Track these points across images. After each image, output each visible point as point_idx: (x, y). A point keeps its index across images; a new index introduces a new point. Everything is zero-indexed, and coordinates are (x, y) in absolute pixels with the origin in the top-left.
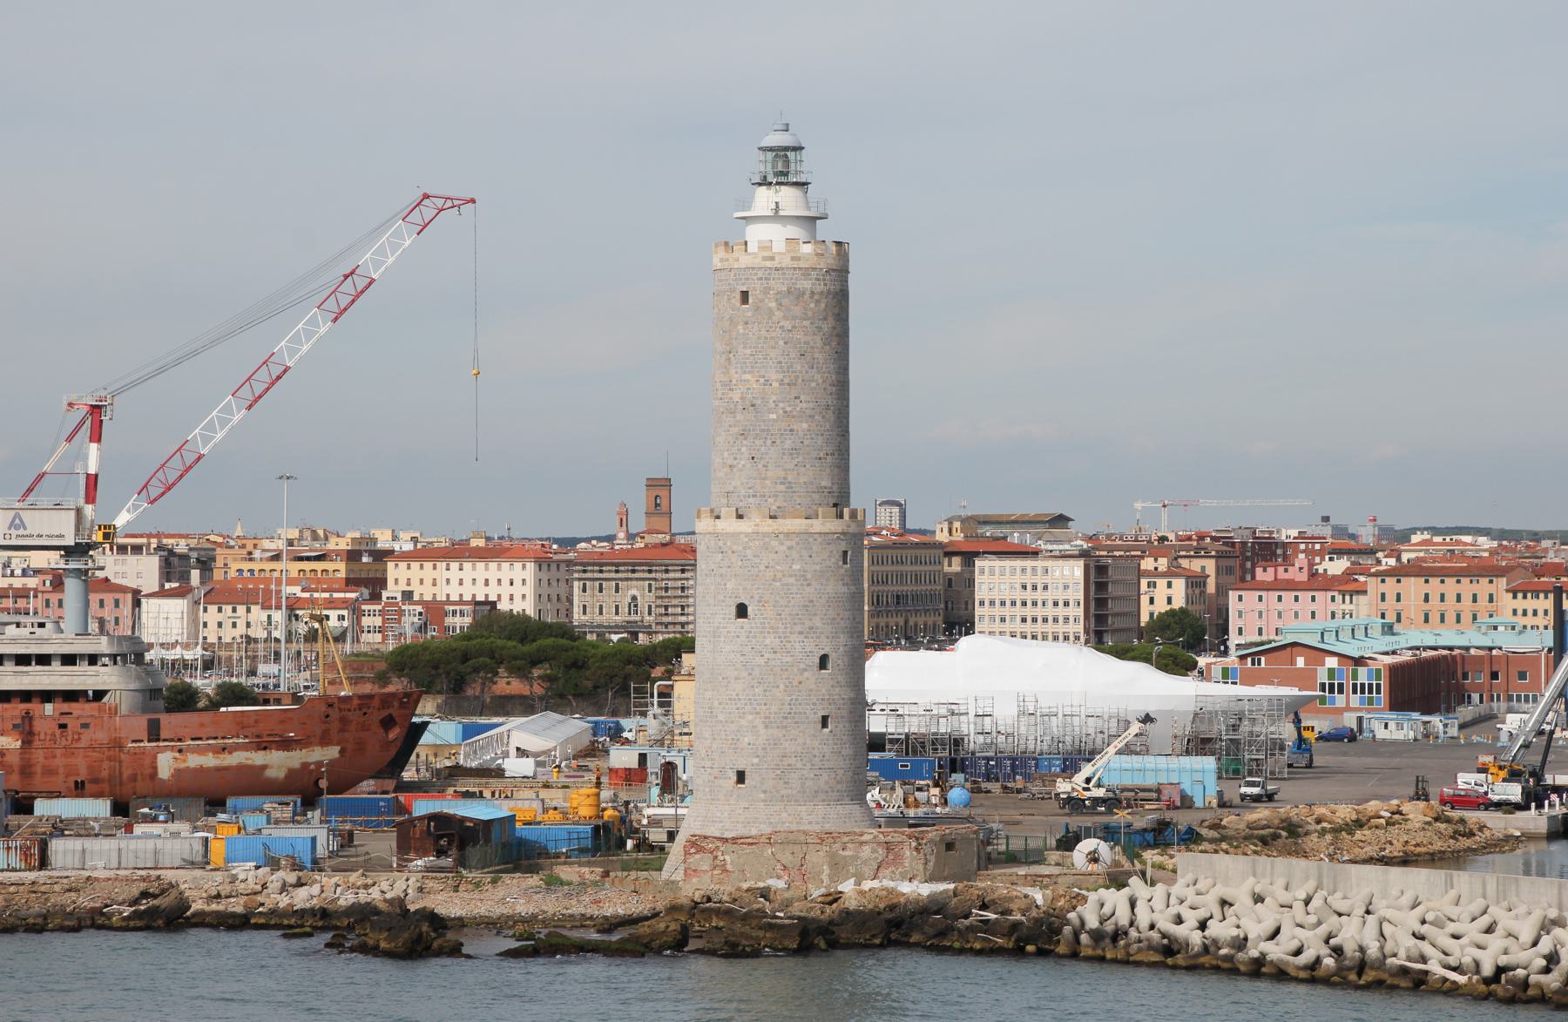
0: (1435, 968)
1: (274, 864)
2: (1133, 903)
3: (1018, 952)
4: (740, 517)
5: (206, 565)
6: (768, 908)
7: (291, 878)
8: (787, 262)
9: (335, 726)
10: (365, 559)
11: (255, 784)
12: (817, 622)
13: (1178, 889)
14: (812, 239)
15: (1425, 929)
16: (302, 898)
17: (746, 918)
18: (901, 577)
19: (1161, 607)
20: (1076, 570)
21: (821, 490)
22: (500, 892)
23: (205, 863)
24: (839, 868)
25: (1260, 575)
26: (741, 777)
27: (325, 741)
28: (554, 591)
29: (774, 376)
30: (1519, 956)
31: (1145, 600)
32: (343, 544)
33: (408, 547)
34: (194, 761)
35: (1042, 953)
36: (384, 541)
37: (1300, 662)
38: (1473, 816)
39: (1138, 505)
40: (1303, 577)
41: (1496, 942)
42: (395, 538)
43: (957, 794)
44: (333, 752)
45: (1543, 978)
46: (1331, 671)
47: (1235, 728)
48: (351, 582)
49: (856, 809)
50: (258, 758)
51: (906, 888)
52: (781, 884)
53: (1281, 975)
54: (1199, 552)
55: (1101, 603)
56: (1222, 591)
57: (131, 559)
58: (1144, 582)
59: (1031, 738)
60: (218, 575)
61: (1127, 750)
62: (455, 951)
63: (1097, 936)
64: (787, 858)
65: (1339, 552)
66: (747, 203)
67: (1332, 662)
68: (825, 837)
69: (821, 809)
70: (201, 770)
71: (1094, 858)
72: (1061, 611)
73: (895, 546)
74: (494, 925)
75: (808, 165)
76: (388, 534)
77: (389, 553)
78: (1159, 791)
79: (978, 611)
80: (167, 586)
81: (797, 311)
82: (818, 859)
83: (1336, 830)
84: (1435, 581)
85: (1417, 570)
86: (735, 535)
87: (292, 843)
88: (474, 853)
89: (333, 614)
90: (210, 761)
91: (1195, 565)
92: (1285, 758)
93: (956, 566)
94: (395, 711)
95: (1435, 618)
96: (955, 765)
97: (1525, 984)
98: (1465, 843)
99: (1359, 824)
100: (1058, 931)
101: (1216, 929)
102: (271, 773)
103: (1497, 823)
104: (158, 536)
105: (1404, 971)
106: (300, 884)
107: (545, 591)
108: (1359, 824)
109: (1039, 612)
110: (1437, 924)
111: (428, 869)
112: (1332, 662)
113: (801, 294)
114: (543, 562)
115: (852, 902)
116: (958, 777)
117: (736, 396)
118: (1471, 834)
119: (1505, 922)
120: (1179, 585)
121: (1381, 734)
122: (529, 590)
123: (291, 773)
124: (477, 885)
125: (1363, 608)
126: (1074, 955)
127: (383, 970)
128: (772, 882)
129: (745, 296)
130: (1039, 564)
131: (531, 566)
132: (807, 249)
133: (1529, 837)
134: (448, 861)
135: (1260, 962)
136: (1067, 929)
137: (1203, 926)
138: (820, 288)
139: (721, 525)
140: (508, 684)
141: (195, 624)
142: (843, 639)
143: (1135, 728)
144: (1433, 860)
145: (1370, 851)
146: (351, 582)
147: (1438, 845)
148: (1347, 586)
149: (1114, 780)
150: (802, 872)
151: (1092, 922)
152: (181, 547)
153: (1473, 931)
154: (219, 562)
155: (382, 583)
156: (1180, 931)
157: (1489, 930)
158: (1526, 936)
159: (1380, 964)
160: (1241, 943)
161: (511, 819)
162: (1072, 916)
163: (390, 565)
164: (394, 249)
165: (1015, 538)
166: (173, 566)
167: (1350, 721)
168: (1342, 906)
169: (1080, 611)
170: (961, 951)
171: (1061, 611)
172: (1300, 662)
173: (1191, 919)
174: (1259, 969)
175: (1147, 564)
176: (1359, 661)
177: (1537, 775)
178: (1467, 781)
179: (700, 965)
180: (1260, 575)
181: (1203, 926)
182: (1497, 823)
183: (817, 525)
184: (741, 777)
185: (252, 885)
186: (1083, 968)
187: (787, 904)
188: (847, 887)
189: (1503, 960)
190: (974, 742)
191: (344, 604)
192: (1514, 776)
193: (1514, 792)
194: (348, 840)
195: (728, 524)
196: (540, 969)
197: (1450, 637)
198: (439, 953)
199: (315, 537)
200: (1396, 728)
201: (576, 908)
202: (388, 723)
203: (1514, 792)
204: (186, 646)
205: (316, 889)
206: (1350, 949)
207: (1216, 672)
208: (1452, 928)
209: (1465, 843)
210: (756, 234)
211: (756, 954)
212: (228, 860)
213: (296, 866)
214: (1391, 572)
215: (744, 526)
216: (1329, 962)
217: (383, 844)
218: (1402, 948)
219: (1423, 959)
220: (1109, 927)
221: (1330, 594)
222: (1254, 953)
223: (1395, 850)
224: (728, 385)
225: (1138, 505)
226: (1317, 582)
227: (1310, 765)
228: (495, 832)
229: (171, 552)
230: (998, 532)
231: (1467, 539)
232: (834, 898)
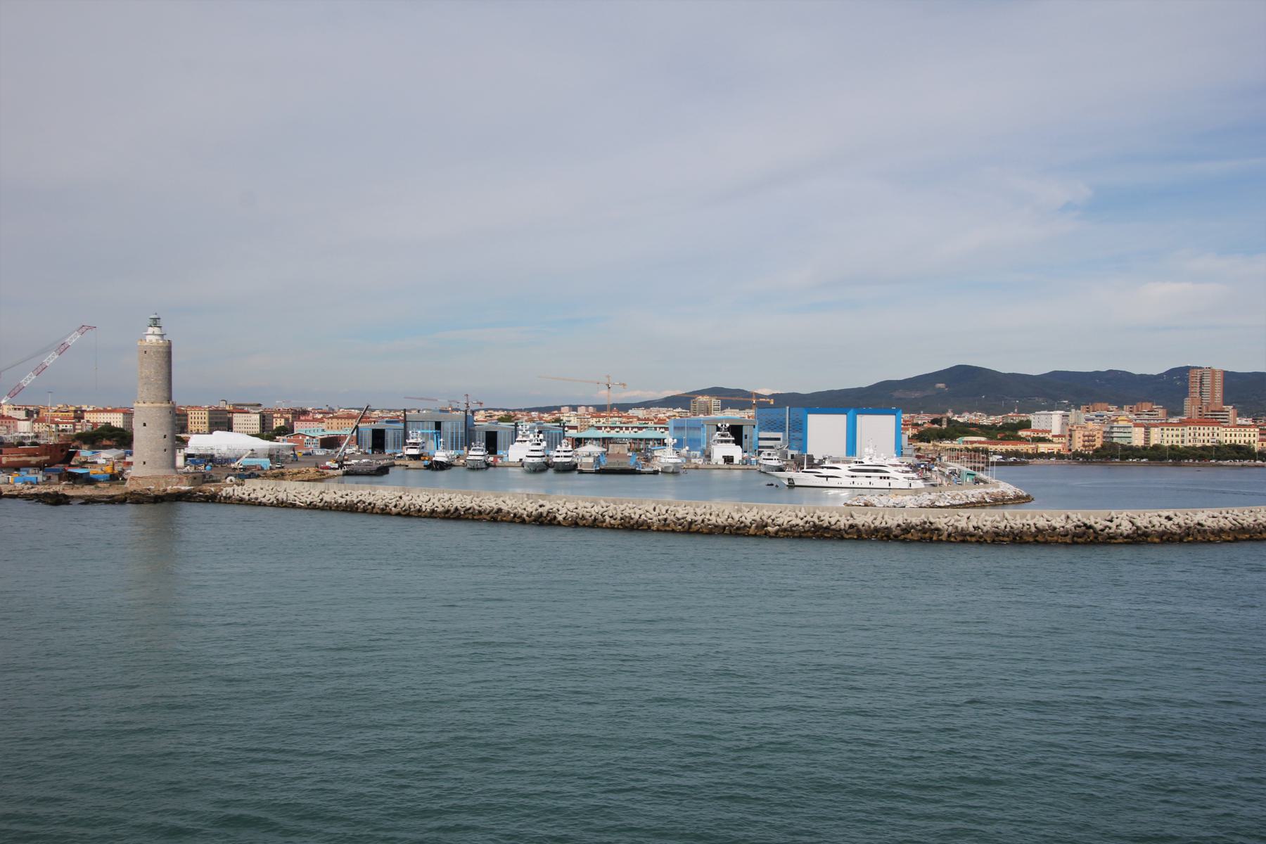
0: (297, 503)
1: (26, 483)
2: (234, 490)
3: (207, 502)
4: (144, 403)
5: (38, 413)
6: (149, 492)
7: (30, 486)
8: (156, 344)
9: (49, 451)
10: (79, 412)
11: (27, 465)
12: (163, 427)
13: (244, 487)
14: (163, 340)
15: (296, 494)
16: (32, 491)
17: (143, 495)
18: (217, 418)
19: (278, 425)
20: (258, 417)
21: (164, 397)
22: (84, 489)
23: (8, 483)
24: (168, 484)
25: (301, 418)
27: (46, 455)
28: (128, 420)
29: (153, 370)
30: (315, 499)
31: (274, 424)
32: (73, 409)
33: (91, 409)
34: (12, 459)
35: (213, 502)
36: (84, 407)
37: (300, 438)
38: (325, 471)
39: (277, 402)
40: (312, 419)
41: (311, 497)
42: (88, 407)
43: (208, 467)
44: (48, 458)
45: (262, 499)
46: (307, 440)
47: (278, 452)
48: (75, 418)
49: (173, 470)
50: (28, 459)
51: (183, 488)
52: (153, 487)
53: (265, 505)
54: (288, 412)
55: (264, 424)
56: (293, 422)
57: (18, 411)
58: (274, 420)
59: (232, 456)
60: (41, 416)
61: (249, 457)
62: (68, 503)
63: (225, 498)
64: (155, 481)
65: (320, 413)
66: (146, 331)
67: (308, 438)
68: (165, 476)
69: (165, 470)
70: (13, 462)
71: (231, 481)
72: (254, 426)
73: (215, 410)
74: (80, 497)
75: (161, 323)
76: (86, 406)
77: (85, 411)
78: (256, 466)
79: (234, 426)
80: (231, 416)
81: (158, 355)
82: (162, 481)
83: (293, 474)
84: (340, 420)
85: (337, 418)
87: (31, 478)
88: (78, 481)
89: (68, 425)
90: (16, 459)
91: (287, 416)
92: (290, 459)
93: (230, 415)
94: (64, 448)
95: (340, 428)
96: (211, 461)
97: (316, 505)
98: (323, 477)
99: (299, 473)
100: (216, 497)
101: (252, 496)
102: (32, 462)
103: (331, 472)
104: (25, 406)
105: (291, 503)
106: (32, 488)
107: (125, 420)
108: (299, 473)
109: (249, 426)
110: (299, 493)
111: (66, 484)
112: (308, 438)
113: (159, 352)
114: (125, 413)
115: (169, 491)
116: (211, 464)
117: (143, 375)
118: (325, 475)
119: (313, 492)
120: (283, 420)
121: (317, 454)
122: (121, 420)
123: (37, 462)
124: (78, 488)
125: (324, 426)
126: (220, 502)
127: (49, 507)
128: (151, 487)
129: (145, 352)
130: (249, 415)
131: (122, 414)
132: (161, 342)
133: (338, 475)
134: (71, 483)
135: (260, 503)
136: (218, 496)
137: (249, 495)
138: (164, 350)
139: (140, 405)
140: (106, 442)
141: (33, 428)
142: (170, 431)
143: (250, 452)
144: (315, 480)
145: (300, 479)
146: (75, 418)
147: (316, 477)
148: (321, 421)
149: (246, 464)
150: (158, 484)
151: (224, 495)
152: (32, 409)
153: (306, 494)
154: (41, 413)
155: (83, 418)
156: (243, 496)
157: (310, 494)
158: (317, 495)
159: (286, 502)
160: (257, 499)
161: (88, 473)
162: (220, 493)
163: (85, 414)
164: (75, 338)
165: (246, 409)
166: (29, 414)
167: (310, 451)
168: (279, 490)
169: (259, 426)
170: (194, 502)
171: (254, 426)
172: (300, 438)
173: (247, 493)
174: (260, 504)
175: (275, 415)
176: (314, 437)
177: (342, 462)
178: (328, 464)
179: (130, 505)
180: (301, 418)
181: (249, 495)
182: (331, 472)
183: (163, 405)
184: (144, 463)
185: (20, 488)
186: (222, 505)
187: (154, 492)
188: (169, 488)
189: (312, 500)
190: (217, 456)
191: (71, 423)
192: (337, 462)
193: (336, 466)
194: (49, 478)
195: (141, 405)
196: (90, 507)
197: (337, 432)
198: (64, 504)
199: (67, 407)
200: (320, 452)
201: (102, 493)
202: (62, 451)
203: (336, 466)
204: (29, 433)
205: (36, 489)
206: (280, 500)
207: (281, 440)
208: (302, 494)
209: (323, 477)
210: (148, 338)
211: (142, 503)
212: (15, 482)
213: (32, 483)
214: (330, 418)
215: (145, 405)
216: (275, 502)
217: (55, 479)
218: (291, 498)
219: (295, 501)
220: (228, 496)
221: (1188, 427)
222: (259, 500)
223: (306, 479)
224: (142, 373)
225: (277, 402)
226: (315, 420)
227: (297, 460)
228: (84, 477)
229: (28, 410)
230: (242, 407)
231: (353, 410)
232: (165, 490)
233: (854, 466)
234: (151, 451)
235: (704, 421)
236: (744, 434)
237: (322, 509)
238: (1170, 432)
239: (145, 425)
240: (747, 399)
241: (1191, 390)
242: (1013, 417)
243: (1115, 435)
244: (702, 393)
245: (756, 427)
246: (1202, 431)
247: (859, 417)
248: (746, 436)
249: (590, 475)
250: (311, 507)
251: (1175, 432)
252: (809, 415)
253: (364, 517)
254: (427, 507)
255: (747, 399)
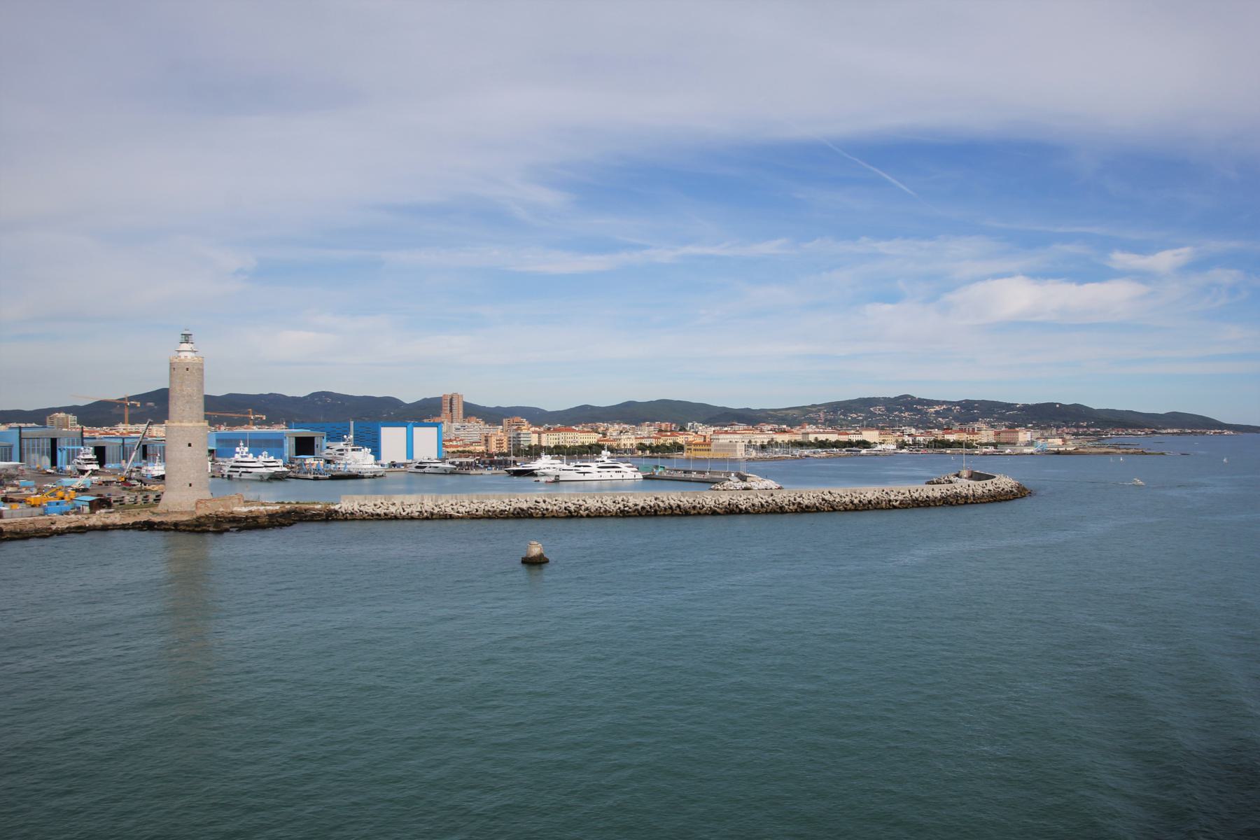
26: (190, 485)
64: (222, 503)
75: (192, 339)
86: (188, 427)
129: (187, 369)
184: (190, 485)
233: (600, 464)
234: (197, 472)
235: (287, 434)
236: (316, 444)
237: (773, 512)
238: (552, 437)
239: (190, 445)
240: (246, 416)
241: (444, 408)
242: (1203, 431)
243: (522, 439)
244: (60, 410)
245: (325, 437)
246: (568, 436)
247: (415, 428)
248: (317, 446)
249: (325, 481)
250: (472, 517)
251: (555, 437)
252: (382, 428)
253: (541, 522)
254: (613, 508)
255: (246, 416)
